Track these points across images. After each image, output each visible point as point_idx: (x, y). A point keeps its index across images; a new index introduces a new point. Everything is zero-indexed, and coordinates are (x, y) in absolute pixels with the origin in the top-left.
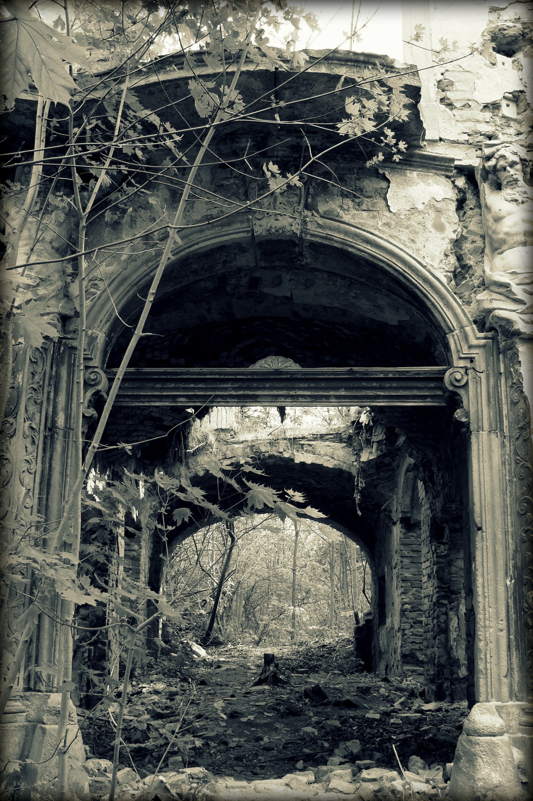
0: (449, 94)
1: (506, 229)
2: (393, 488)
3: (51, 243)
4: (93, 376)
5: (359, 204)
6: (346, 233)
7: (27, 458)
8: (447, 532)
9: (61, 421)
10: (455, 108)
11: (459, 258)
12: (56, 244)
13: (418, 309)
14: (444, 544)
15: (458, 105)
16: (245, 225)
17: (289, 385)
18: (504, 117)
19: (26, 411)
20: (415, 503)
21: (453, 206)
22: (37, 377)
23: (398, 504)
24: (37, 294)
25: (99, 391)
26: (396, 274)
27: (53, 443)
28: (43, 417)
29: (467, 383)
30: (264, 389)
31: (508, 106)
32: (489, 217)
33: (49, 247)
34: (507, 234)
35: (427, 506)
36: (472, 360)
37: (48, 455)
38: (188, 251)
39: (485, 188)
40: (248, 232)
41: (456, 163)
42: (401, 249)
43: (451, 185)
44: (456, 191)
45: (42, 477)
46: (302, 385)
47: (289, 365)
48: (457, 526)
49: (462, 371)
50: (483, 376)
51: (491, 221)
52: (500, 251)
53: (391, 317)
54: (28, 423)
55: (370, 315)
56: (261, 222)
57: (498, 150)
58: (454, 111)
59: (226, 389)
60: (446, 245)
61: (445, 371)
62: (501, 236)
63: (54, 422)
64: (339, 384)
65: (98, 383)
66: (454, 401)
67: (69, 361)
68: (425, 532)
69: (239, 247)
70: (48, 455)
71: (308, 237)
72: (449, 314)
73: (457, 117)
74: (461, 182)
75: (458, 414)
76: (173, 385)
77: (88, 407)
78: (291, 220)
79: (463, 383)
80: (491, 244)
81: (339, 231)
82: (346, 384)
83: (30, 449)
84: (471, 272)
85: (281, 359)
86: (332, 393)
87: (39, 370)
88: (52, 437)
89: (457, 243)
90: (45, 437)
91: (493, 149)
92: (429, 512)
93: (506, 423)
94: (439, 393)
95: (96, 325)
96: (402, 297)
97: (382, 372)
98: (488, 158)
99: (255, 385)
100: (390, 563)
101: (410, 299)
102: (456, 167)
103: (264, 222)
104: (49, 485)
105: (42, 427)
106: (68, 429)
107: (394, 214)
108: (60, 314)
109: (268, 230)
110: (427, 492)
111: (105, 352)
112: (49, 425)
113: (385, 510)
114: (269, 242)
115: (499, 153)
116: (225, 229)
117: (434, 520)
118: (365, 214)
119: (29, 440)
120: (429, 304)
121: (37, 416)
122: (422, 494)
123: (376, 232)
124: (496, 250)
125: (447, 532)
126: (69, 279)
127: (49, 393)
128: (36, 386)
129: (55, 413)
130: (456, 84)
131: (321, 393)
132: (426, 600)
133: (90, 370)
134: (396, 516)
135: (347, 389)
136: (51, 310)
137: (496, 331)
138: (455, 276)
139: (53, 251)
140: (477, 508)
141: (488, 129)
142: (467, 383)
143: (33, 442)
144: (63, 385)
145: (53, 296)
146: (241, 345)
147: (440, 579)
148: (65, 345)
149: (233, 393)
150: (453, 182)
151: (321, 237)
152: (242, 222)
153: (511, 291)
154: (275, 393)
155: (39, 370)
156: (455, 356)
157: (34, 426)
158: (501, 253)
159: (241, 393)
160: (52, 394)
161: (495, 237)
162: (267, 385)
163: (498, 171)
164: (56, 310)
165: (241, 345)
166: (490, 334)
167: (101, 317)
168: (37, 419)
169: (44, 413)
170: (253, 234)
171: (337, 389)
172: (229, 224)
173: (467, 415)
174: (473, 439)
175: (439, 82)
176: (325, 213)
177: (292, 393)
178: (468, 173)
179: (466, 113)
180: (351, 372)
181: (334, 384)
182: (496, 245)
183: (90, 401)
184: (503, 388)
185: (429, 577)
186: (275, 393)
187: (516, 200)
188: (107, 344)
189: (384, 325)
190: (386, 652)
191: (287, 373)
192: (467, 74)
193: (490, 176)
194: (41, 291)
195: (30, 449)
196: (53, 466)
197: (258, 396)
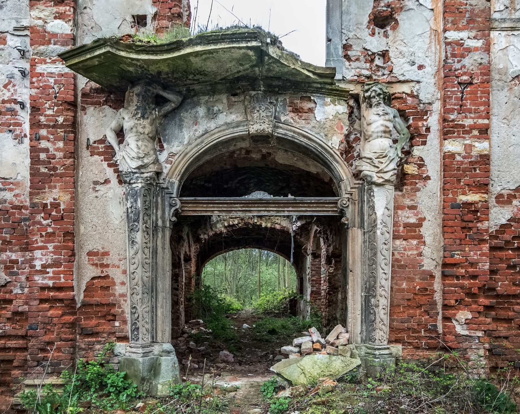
0: (349, 53)
1: (372, 130)
2: (308, 239)
3: (148, 134)
4: (174, 202)
5: (301, 117)
6: (294, 132)
7: (146, 241)
8: (333, 261)
9: (160, 223)
10: (352, 61)
11: (348, 142)
12: (150, 135)
13: (327, 168)
14: (332, 267)
15: (353, 59)
16: (246, 127)
17: (266, 205)
18: (376, 65)
19: (143, 219)
20: (318, 246)
21: (347, 116)
22: (147, 203)
23: (310, 247)
24: (144, 162)
25: (177, 209)
26: (317, 153)
27: (157, 234)
28: (151, 222)
29: (348, 206)
30: (255, 207)
31: (379, 59)
32: (365, 123)
33: (147, 136)
34: (373, 132)
35: (324, 250)
36: (351, 194)
37: (155, 239)
38: (217, 140)
39: (363, 106)
40: (246, 131)
41: (351, 92)
42: (321, 140)
43: (346, 105)
44: (349, 108)
45: (153, 249)
46: (272, 206)
47: (267, 196)
48: (338, 259)
49: (346, 200)
50: (357, 202)
51: (365, 125)
52: (368, 140)
53: (313, 170)
54: (144, 225)
55: (304, 168)
56: (253, 126)
57: (372, 87)
58: (351, 63)
59: (237, 207)
60: (342, 137)
61: (339, 199)
62: (370, 133)
63: (157, 224)
64: (289, 205)
65: (176, 205)
66: (342, 213)
67: (162, 195)
68: (323, 261)
69: (242, 138)
70: (155, 239)
71: (276, 134)
72: (341, 171)
73: (352, 66)
74: (352, 102)
75: (343, 220)
76: (212, 205)
77: (172, 217)
78: (268, 126)
79: (346, 206)
80: (364, 136)
81: (290, 131)
82: (292, 205)
83: (147, 237)
84: (353, 149)
85: (262, 192)
86: (286, 209)
87: (148, 199)
88: (156, 230)
89: (347, 136)
90: (153, 231)
91: (370, 86)
92: (325, 253)
93: (366, 224)
94: (335, 209)
95: (174, 177)
96: (320, 163)
97: (309, 200)
98: (367, 91)
99: (250, 205)
100: (305, 272)
101: (323, 164)
102: (351, 95)
103: (254, 126)
104: (156, 253)
105: (151, 227)
106: (164, 227)
107: (318, 121)
108: (155, 172)
109: (257, 131)
110: (324, 243)
111: (178, 189)
112: (154, 225)
113: (304, 249)
114: (257, 136)
115: (373, 89)
116: (235, 129)
117: (327, 256)
118: (303, 121)
119: (146, 233)
120: (332, 167)
121: (149, 221)
122: (322, 244)
123: (309, 132)
124: (367, 139)
125: (333, 261)
126: (158, 153)
127: (153, 210)
128: (147, 207)
129: (157, 220)
130: (354, 47)
131: (281, 209)
132: (323, 291)
133: (172, 199)
134: (309, 252)
135: (292, 207)
136: (151, 170)
137: (364, 180)
138: (346, 152)
139: (149, 139)
140: (350, 262)
141: (367, 73)
142: (348, 206)
143: (148, 234)
144: (160, 206)
145: (152, 163)
146: (239, 178)
147: (330, 283)
148: (159, 187)
149: (240, 209)
150: (348, 103)
151: (282, 134)
152: (243, 126)
153: (372, 162)
154: (259, 209)
155: (148, 199)
156: (344, 192)
157: (147, 226)
158: (369, 141)
159: (244, 209)
160: (155, 211)
161: (366, 133)
162: (256, 206)
163: (371, 98)
164: (154, 170)
165: (239, 178)
166: (361, 182)
167: (176, 173)
168: (149, 223)
169: (151, 220)
170: (249, 132)
171: (288, 207)
172: (237, 127)
173: (347, 220)
174: (350, 231)
175: (344, 45)
176: (284, 121)
177: (268, 209)
178: (356, 98)
179: (357, 64)
180: (295, 200)
181: (287, 205)
182: (367, 137)
183: (173, 214)
184: (366, 208)
185: (325, 281)
186: (259, 209)
187: (379, 114)
188: (179, 186)
189: (308, 173)
190: (303, 311)
191: (265, 200)
192: (359, 40)
193: (367, 100)
194: (146, 161)
195: (147, 237)
196: (158, 244)
197: (252, 211)
